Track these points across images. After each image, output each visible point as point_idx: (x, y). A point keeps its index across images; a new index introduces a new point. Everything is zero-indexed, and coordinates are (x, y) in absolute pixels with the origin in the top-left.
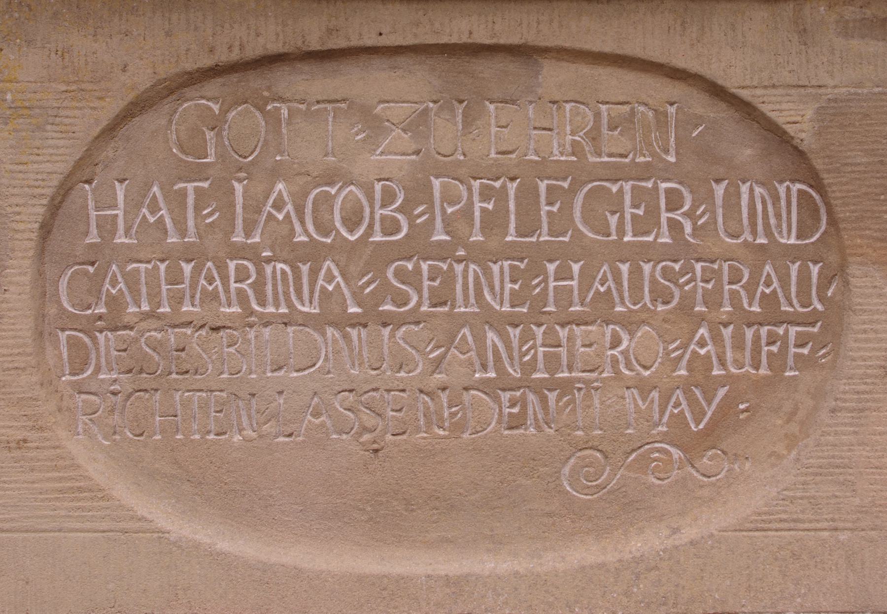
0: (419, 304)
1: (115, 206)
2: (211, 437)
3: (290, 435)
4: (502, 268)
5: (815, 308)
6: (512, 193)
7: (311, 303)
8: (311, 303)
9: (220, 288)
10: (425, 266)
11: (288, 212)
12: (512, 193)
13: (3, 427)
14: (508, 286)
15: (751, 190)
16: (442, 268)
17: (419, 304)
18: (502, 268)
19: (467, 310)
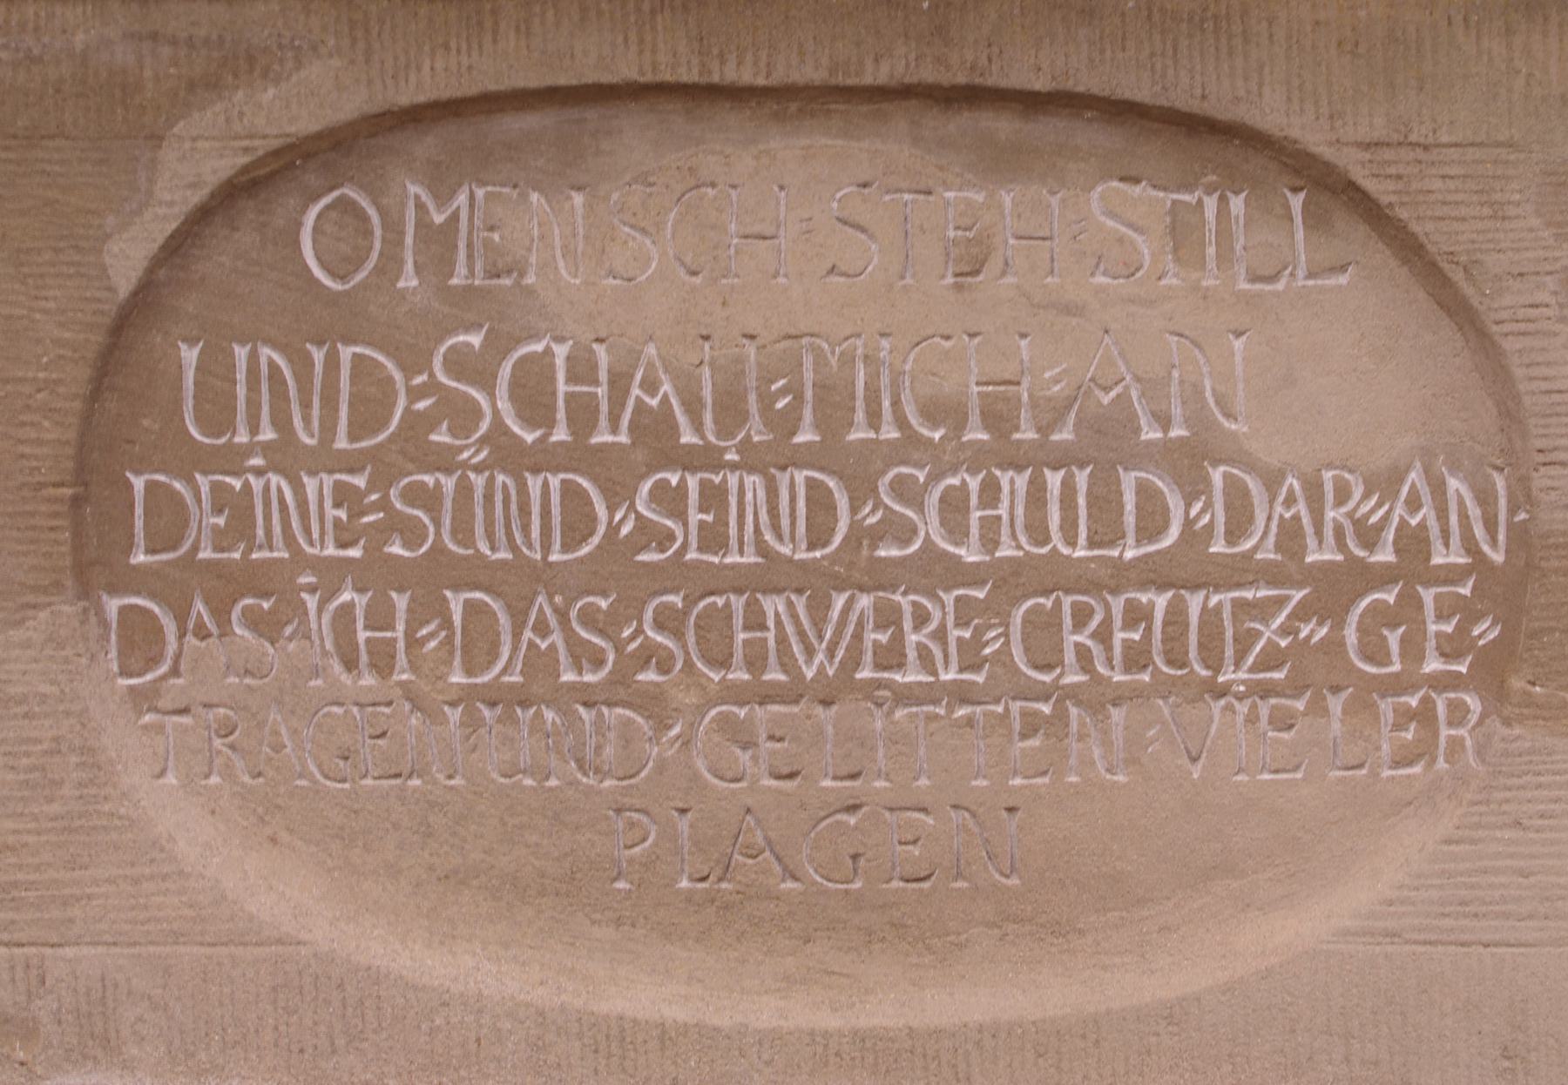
0: (685, 546)
1: (596, 383)
2: (369, 782)
3: (853, 776)
4: (546, 484)
5: (1054, 549)
6: (560, 362)
7: (1447, 545)
8: (1447, 545)
9: (1433, 524)
10: (692, 482)
11: (666, 395)
12: (560, 362)
13: (1566, 772)
14: (331, 512)
15: (253, 357)
16: (233, 488)
17: (685, 546)
18: (546, 484)
19: (744, 560)
